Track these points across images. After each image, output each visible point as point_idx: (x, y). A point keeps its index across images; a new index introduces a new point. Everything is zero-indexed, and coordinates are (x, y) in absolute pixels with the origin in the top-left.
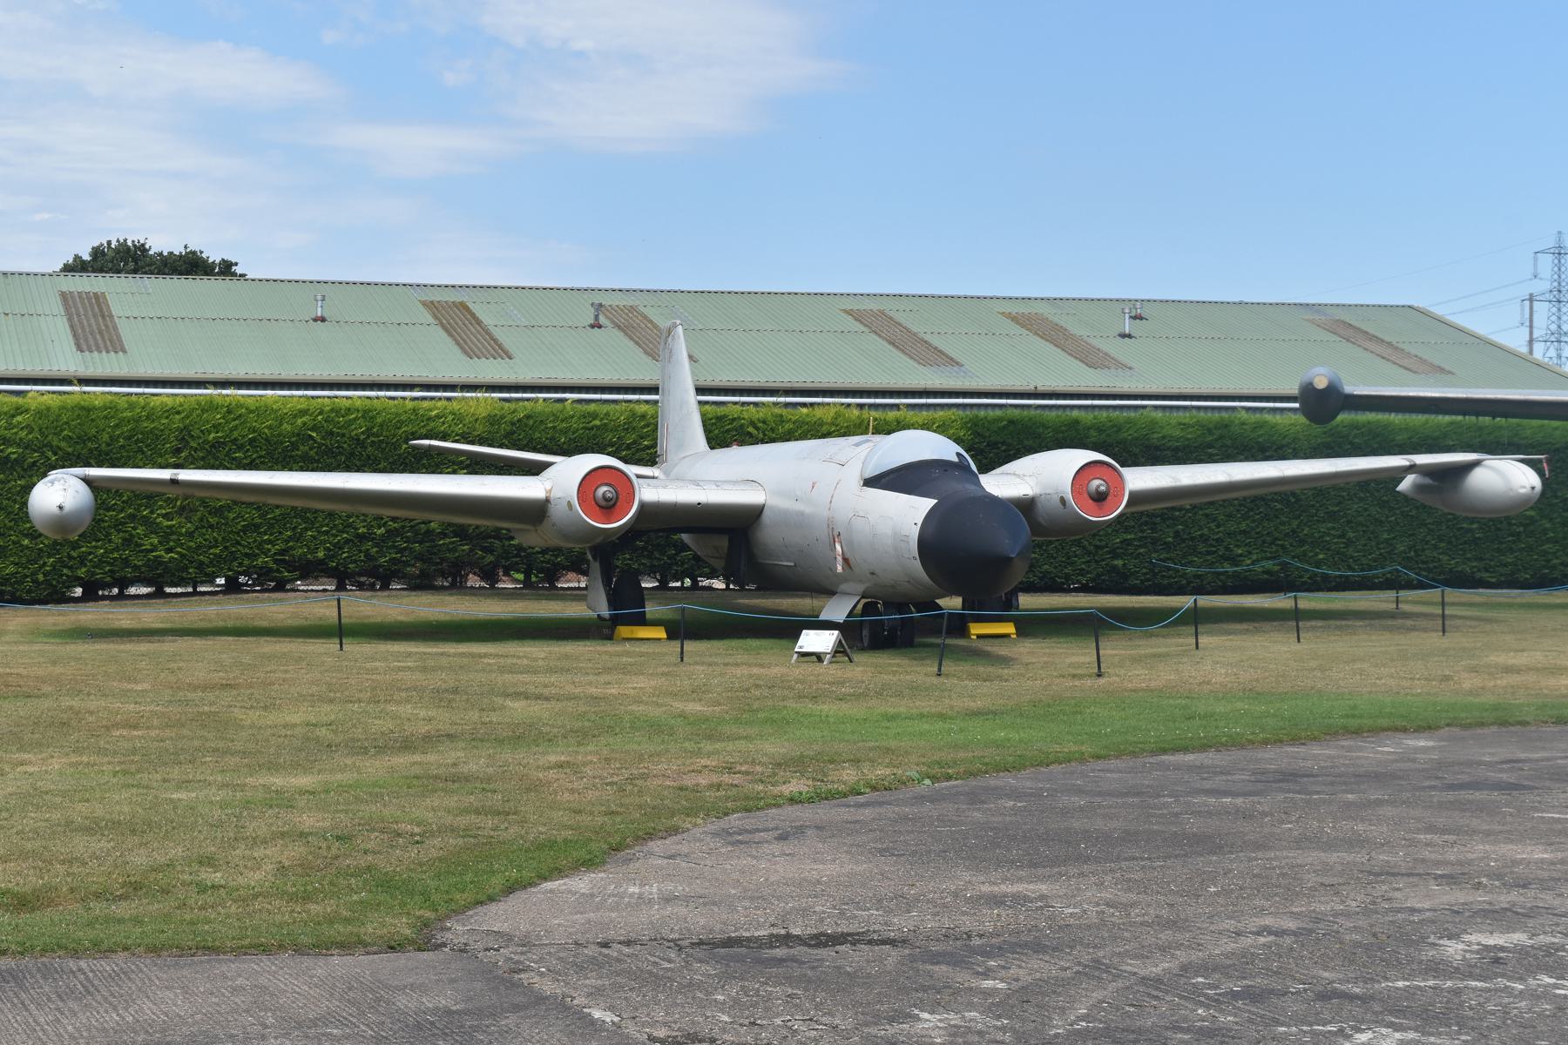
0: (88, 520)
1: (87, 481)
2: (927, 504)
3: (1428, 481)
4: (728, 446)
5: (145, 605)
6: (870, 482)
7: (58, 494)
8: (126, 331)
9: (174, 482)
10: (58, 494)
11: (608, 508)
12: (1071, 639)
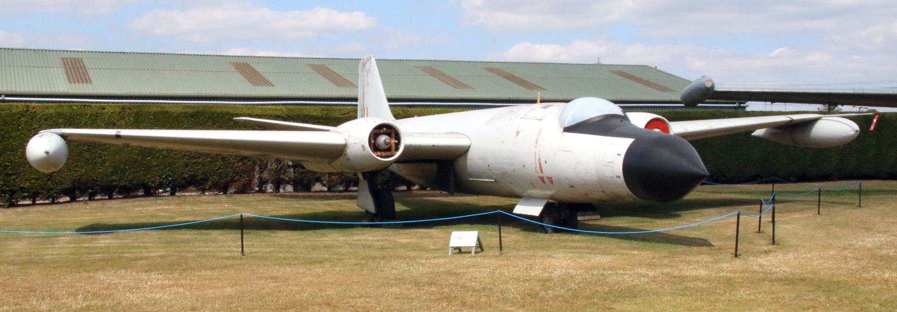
0: (64, 160)
1: (63, 136)
2: (632, 140)
3: (775, 131)
4: (413, 116)
5: (101, 222)
6: (568, 129)
7: (43, 145)
8: (91, 74)
9: (118, 137)
10: (43, 145)
11: (388, 150)
12: (490, 226)
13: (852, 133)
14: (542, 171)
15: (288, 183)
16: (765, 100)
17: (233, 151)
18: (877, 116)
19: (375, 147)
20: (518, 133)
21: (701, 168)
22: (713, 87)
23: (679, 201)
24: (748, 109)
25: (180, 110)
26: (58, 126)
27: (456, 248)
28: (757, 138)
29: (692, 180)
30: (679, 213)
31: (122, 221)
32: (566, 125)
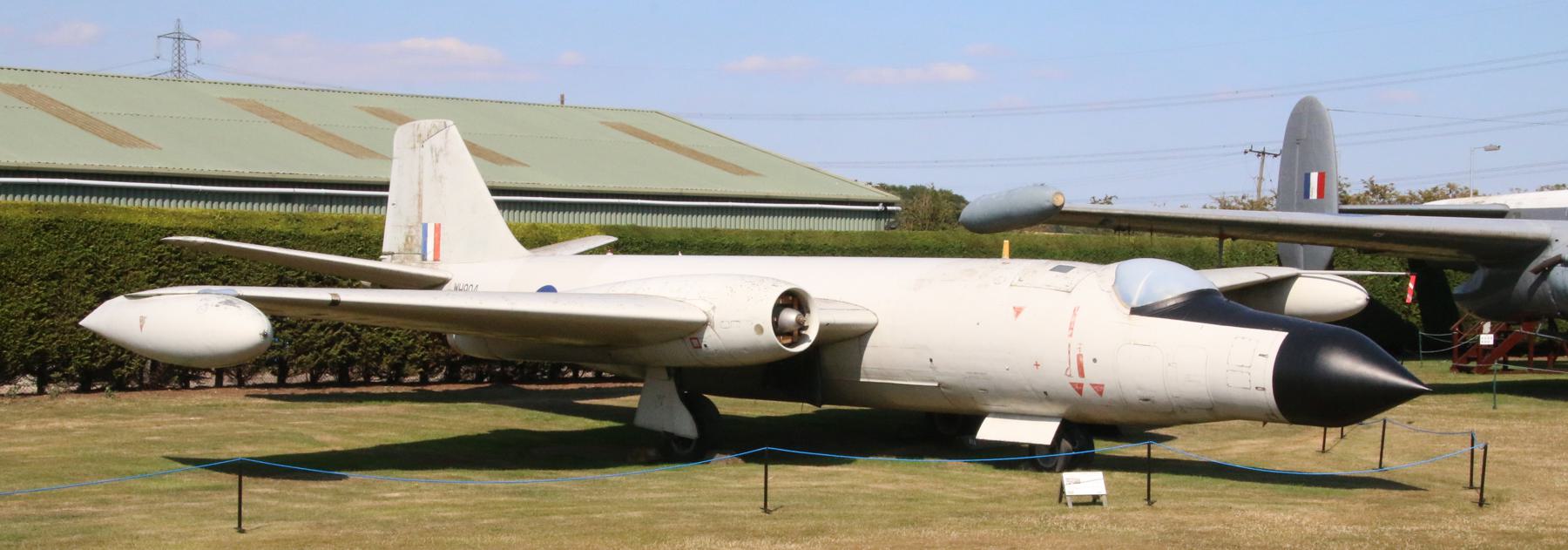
6: (1135, 311)
9: (335, 304)
14: (1082, 374)
15: (24, 373)
17: (421, 325)
19: (779, 330)
20: (1018, 311)
25: (26, 215)
26: (245, 281)
32: (1135, 304)
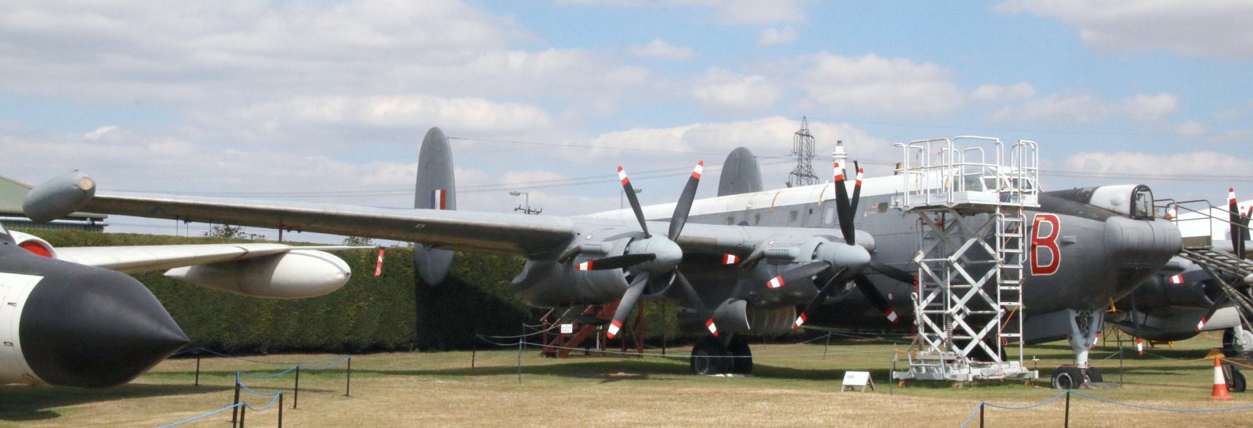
2: (37, 279)
13: (341, 276)
16: (177, 217)
18: (382, 252)
21: (171, 329)
22: (93, 190)
23: (123, 385)
24: (106, 230)
27: (848, 386)
28: (175, 281)
29: (147, 351)
30: (53, 409)
31: (398, 369)
